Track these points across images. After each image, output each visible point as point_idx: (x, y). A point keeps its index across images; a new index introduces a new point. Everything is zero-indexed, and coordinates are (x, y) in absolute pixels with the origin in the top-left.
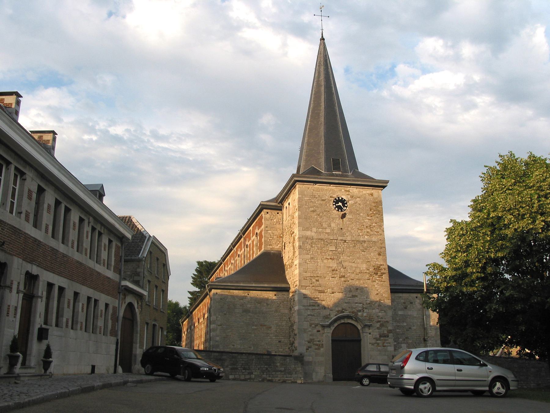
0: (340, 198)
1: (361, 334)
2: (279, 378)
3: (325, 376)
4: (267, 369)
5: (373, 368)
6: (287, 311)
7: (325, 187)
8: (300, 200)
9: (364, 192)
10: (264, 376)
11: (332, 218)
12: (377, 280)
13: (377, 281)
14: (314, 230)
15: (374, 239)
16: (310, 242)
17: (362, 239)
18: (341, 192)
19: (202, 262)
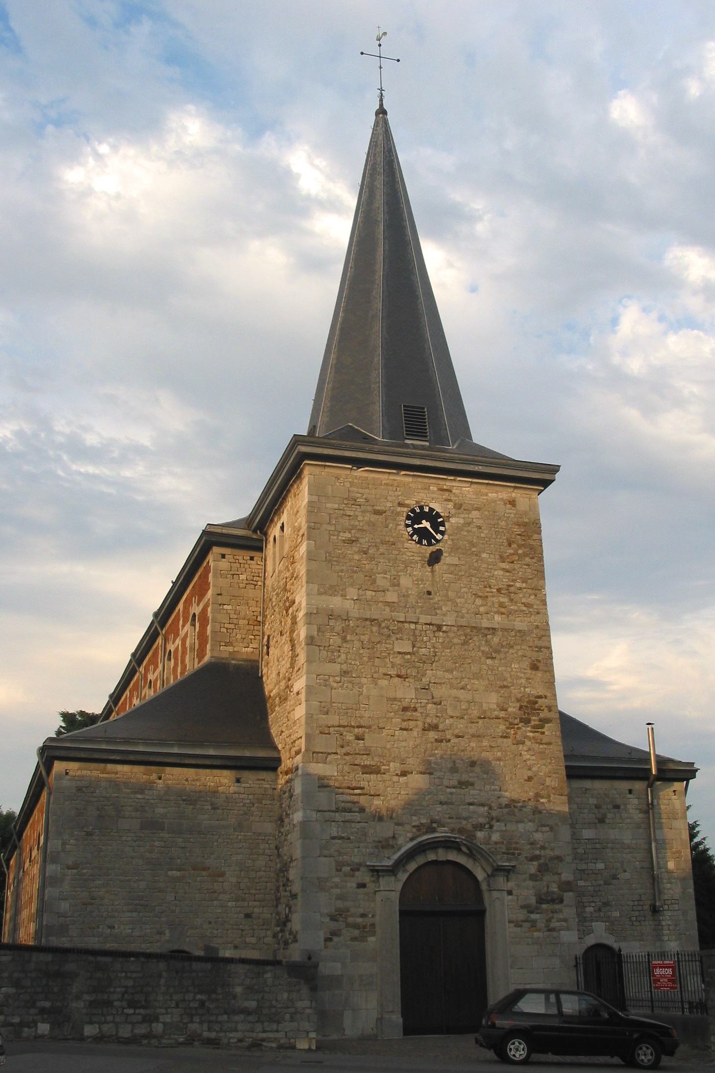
0: (426, 510)
1: (486, 895)
2: (239, 1035)
3: (380, 1020)
4: (202, 1003)
5: (533, 1005)
6: (269, 827)
7: (384, 476)
8: (312, 508)
9: (492, 495)
10: (194, 1027)
11: (404, 562)
12: (529, 738)
13: (528, 743)
14: (353, 593)
15: (520, 624)
16: (338, 626)
17: (485, 624)
18: (427, 492)
19: (73, 715)
